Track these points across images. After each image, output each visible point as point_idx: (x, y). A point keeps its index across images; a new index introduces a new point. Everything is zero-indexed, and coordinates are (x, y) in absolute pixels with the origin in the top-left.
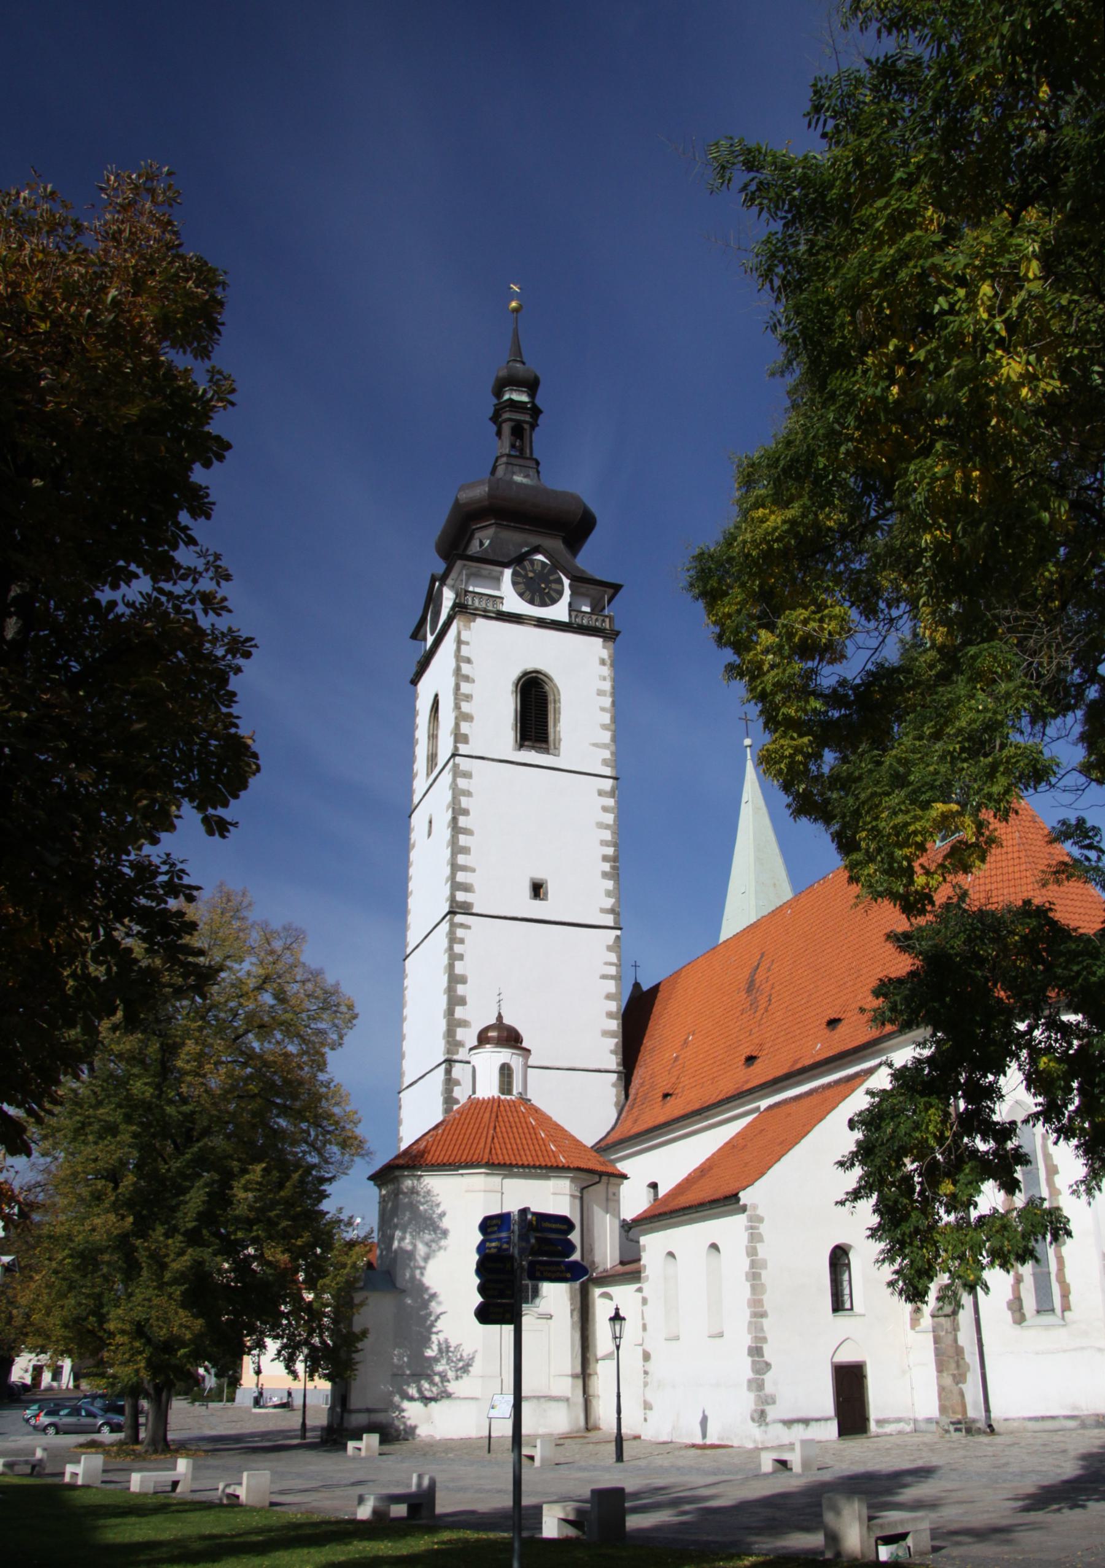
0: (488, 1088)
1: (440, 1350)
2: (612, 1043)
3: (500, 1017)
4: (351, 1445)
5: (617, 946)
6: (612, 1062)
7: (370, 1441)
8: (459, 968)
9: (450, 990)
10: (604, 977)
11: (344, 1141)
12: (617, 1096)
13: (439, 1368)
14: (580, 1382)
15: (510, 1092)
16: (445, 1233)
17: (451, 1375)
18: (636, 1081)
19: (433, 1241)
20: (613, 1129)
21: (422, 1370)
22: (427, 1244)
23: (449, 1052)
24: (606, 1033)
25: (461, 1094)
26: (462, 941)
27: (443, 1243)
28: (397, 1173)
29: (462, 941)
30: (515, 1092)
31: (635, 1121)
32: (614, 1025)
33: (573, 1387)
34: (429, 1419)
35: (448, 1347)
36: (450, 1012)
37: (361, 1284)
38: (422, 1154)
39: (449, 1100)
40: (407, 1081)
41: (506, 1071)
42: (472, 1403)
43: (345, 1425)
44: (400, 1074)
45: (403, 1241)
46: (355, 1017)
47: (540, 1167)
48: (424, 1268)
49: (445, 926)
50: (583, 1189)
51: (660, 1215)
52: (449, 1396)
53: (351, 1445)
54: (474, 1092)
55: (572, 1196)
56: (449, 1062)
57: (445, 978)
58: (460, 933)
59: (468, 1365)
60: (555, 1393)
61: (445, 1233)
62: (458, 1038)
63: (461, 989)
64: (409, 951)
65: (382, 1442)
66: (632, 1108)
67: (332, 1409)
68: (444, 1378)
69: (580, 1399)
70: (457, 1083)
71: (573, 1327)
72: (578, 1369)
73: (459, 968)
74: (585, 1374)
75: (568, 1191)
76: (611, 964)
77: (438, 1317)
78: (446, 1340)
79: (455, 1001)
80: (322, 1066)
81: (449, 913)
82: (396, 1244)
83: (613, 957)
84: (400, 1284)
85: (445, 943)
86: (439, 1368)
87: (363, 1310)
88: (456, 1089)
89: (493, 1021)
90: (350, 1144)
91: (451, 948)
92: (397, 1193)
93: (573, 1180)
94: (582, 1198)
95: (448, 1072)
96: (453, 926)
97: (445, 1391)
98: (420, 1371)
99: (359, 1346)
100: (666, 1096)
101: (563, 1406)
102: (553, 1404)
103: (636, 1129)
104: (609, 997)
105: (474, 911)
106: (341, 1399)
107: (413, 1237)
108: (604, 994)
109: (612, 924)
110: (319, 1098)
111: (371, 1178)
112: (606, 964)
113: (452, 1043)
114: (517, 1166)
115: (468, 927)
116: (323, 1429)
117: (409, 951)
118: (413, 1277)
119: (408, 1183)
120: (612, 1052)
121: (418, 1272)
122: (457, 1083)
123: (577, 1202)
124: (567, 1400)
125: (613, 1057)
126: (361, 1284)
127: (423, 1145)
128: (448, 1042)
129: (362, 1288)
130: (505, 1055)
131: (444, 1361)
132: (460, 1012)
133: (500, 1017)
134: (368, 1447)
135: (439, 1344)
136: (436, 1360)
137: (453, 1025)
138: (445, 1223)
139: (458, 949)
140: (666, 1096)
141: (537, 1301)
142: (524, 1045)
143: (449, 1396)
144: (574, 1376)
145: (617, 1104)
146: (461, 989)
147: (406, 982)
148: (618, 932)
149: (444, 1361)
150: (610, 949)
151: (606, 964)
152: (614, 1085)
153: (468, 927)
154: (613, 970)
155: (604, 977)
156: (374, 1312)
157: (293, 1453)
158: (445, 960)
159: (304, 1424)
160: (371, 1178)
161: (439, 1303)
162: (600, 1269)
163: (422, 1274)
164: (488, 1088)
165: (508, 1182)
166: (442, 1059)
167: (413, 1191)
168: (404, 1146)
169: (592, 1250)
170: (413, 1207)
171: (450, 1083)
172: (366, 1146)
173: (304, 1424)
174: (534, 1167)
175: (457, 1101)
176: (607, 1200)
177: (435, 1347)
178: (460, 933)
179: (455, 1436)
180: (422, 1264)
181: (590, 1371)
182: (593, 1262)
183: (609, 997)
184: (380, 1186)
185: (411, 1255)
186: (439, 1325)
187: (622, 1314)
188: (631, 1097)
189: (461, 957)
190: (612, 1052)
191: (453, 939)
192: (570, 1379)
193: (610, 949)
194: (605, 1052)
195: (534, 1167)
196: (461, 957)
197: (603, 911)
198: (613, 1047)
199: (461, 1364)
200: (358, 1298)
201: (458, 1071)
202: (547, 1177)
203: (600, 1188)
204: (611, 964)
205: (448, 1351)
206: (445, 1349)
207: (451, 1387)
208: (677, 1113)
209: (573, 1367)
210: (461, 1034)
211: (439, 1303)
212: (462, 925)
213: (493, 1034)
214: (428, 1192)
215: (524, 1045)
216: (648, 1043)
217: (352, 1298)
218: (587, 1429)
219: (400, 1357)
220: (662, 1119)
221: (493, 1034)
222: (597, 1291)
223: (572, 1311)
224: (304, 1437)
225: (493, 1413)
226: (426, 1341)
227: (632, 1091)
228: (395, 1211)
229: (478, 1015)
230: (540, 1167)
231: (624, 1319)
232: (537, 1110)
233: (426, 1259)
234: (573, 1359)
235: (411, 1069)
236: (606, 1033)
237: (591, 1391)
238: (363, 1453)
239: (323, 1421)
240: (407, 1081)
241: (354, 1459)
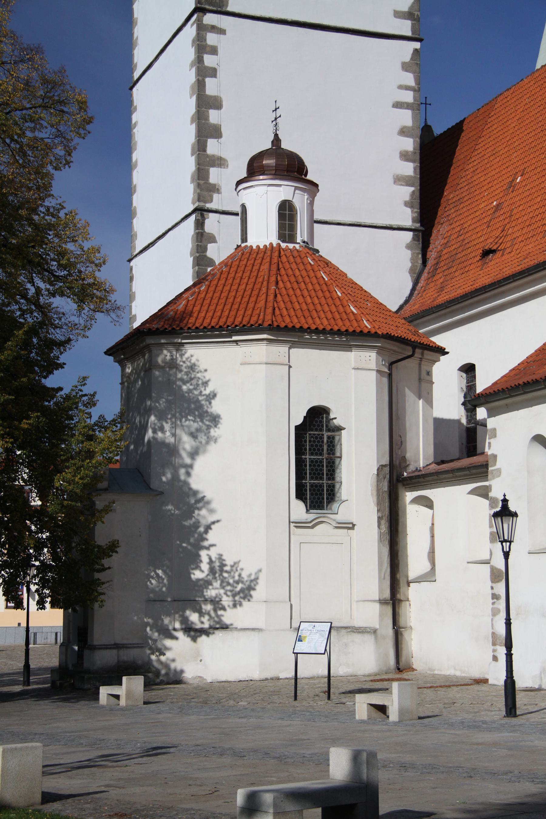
0: (263, 232)
1: (212, 571)
2: (407, 192)
3: (277, 140)
4: (104, 691)
5: (418, 64)
6: (407, 217)
7: (131, 686)
8: (212, 87)
9: (200, 117)
10: (398, 105)
11: (83, 289)
12: (413, 260)
13: (211, 593)
14: (389, 610)
15: (292, 239)
16: (215, 420)
17: (226, 601)
18: (437, 242)
19: (198, 430)
20: (407, 302)
21: (188, 596)
22: (193, 436)
23: (200, 198)
24: (399, 180)
25: (219, 252)
26: (214, 51)
27: (214, 432)
28: (150, 340)
29: (214, 51)
30: (299, 240)
31: (442, 289)
32: (409, 169)
33: (381, 615)
34: (198, 657)
35: (222, 565)
36: (200, 147)
37: (104, 484)
38: (186, 314)
39: (200, 259)
40: (139, 245)
41: (286, 212)
42: (254, 636)
43: (86, 665)
44: (131, 237)
45: (162, 431)
46: (89, 121)
47: (339, 333)
48: (191, 466)
49: (190, 31)
50: (391, 364)
51: (526, 384)
52: (225, 627)
53: (104, 691)
54: (244, 239)
55: (378, 371)
56: (201, 212)
57: (193, 101)
58: (211, 39)
59: (251, 588)
60: (358, 623)
61: (215, 420)
62: (213, 179)
63: (214, 116)
64: (136, 75)
65: (148, 685)
66: (433, 274)
67: (65, 646)
68: (216, 603)
69: (390, 632)
70: (212, 239)
71: (380, 540)
72: (387, 594)
73: (212, 87)
74: (394, 600)
75: (373, 366)
76: (407, 88)
77: (208, 528)
78: (220, 557)
79: (206, 131)
80: (45, 189)
81: (196, 10)
82: (150, 434)
83: (409, 79)
84: (154, 485)
85: (191, 54)
86: (211, 593)
87: (107, 518)
88: (210, 246)
89: (269, 146)
90: (93, 295)
91: (199, 60)
92: (149, 368)
93: (380, 351)
94: (390, 376)
95: (200, 224)
96: (202, 29)
97: (220, 622)
98: (186, 599)
99: (106, 562)
100: (487, 253)
101: (369, 639)
102: (357, 637)
103: (443, 298)
104: (403, 132)
105: (230, 9)
106: (78, 632)
107: (174, 426)
108: (397, 129)
109: (409, 34)
110: (41, 231)
111: (109, 352)
112: (401, 87)
113: (204, 188)
114: (309, 330)
115: (222, 32)
116: (53, 670)
117: (136, 75)
118: (175, 477)
119: (166, 355)
120: (406, 204)
121: (182, 471)
122: (212, 239)
123: (385, 380)
124: (375, 631)
125: (408, 211)
126: (104, 484)
127: (181, 306)
128: (199, 186)
129: (106, 490)
130: (285, 190)
131: (217, 584)
132: (213, 147)
133: (277, 140)
134: (129, 694)
135: (211, 562)
136: (207, 583)
137: (205, 163)
138: (216, 407)
139: (209, 60)
140: (487, 253)
141: (335, 506)
142: (309, 177)
143: (225, 627)
144: (382, 602)
145: (412, 271)
146: (214, 116)
147: (135, 118)
148: (417, 45)
149: (217, 584)
150: (405, 67)
151: (401, 87)
152: (408, 247)
153: (222, 32)
154: (409, 97)
155: (398, 105)
156: (122, 520)
157: (22, 704)
158: (191, 76)
159: (27, 665)
160: (109, 352)
161: (212, 511)
162: (411, 468)
163: (188, 474)
164: (263, 232)
165: (297, 352)
166: (191, 208)
167: (173, 365)
168: (136, 325)
169: (402, 443)
170: (170, 386)
171: (202, 239)
172: (112, 297)
173: (27, 665)
174: (332, 332)
175: (211, 262)
176: (420, 380)
177: (205, 566)
178: (211, 39)
179: (231, 678)
180: (188, 461)
181: (400, 596)
182: (404, 458)
183: (403, 132)
184: (122, 363)
185: (173, 450)
186: (212, 537)
187: (512, 507)
188: (431, 262)
189: (213, 72)
190: (406, 204)
191: (202, 48)
192: (377, 606)
193: (405, 67)
194: (398, 205)
195: (332, 332)
196: (213, 72)
197: (398, 14)
198: (407, 198)
199: (239, 587)
200: (100, 503)
201: (212, 223)
202: (348, 348)
203: (412, 363)
204: (407, 88)
205: (222, 571)
206: (218, 569)
207: (228, 617)
208: (508, 271)
209: (381, 591)
210: (215, 175)
211: (212, 511)
212: (214, 29)
213: (269, 162)
214: (192, 367)
215: (309, 177)
216: (449, 195)
217: (93, 503)
218: (399, 670)
219: (158, 580)
220: (486, 280)
221: (269, 162)
222: (409, 496)
223: (380, 519)
224: (27, 682)
225: (301, 647)
226: (194, 560)
227: (432, 255)
228: (146, 392)
229: (238, 146)
230: (339, 333)
231: (515, 515)
232: (327, 263)
233: (194, 454)
234: (381, 580)
235: (144, 229)
236: (399, 180)
237: (402, 622)
238: (123, 702)
239: (54, 661)
240: (139, 245)
241: (112, 710)
